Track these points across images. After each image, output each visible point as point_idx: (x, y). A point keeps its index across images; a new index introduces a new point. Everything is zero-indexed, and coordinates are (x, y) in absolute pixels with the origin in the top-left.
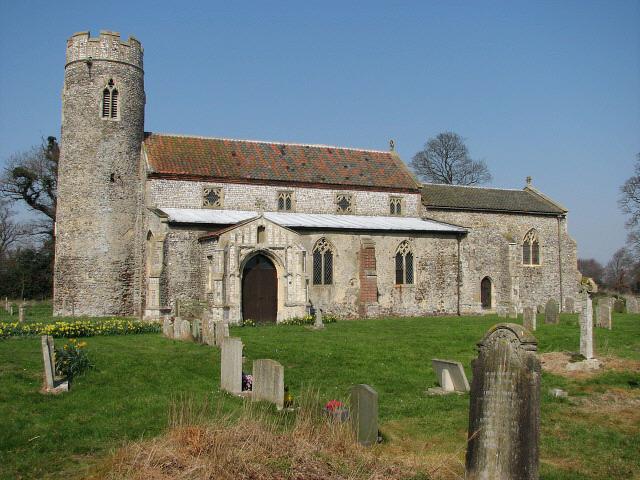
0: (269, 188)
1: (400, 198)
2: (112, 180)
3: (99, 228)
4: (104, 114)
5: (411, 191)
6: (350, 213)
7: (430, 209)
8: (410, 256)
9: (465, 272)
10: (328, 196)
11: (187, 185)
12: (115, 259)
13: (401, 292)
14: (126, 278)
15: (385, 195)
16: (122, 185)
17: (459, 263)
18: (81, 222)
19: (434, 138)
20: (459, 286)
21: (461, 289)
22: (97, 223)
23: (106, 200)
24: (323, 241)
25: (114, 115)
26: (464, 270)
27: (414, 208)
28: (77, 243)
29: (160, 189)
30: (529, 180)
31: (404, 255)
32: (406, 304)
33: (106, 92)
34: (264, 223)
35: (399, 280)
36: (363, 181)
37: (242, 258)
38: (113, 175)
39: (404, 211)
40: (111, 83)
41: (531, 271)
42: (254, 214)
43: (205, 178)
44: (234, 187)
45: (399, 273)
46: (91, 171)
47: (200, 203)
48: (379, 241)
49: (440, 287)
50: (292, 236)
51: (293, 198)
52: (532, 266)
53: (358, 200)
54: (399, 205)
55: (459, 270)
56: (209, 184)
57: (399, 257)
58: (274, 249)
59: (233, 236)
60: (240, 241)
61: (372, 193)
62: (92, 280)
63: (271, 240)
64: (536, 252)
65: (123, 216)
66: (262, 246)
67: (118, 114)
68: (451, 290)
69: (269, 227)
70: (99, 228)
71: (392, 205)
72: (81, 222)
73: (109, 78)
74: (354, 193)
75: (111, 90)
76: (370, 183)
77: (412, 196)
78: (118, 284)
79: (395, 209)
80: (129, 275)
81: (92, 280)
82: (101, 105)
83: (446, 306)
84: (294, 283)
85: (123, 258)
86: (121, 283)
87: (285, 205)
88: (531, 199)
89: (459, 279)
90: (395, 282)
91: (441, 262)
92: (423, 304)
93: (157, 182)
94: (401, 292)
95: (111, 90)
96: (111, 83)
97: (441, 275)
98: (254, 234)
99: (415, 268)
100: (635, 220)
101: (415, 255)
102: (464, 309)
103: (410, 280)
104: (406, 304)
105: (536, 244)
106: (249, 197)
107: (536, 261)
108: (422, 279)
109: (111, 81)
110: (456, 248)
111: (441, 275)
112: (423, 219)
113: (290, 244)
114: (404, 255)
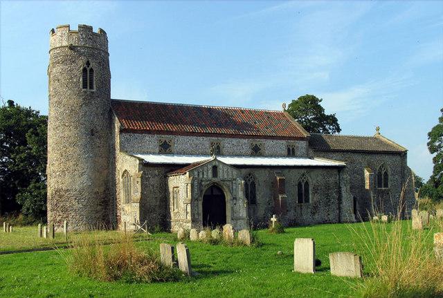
0: (205, 139)
8: (307, 184)
9: (344, 194)
11: (147, 137)
15: (284, 142)
19: (296, 99)
21: (341, 205)
24: (250, 175)
25: (91, 87)
27: (304, 151)
30: (378, 129)
33: (85, 70)
34: (217, 163)
35: (300, 201)
37: (205, 189)
38: (92, 130)
39: (298, 153)
41: (383, 192)
42: (211, 158)
44: (181, 138)
45: (300, 195)
48: (257, 173)
49: (327, 204)
50: (235, 172)
51: (221, 146)
53: (266, 146)
55: (339, 193)
57: (300, 185)
58: (224, 181)
60: (201, 176)
61: (275, 141)
65: (100, 160)
66: (215, 180)
68: (334, 207)
71: (289, 150)
74: (263, 141)
75: (88, 69)
76: (274, 134)
77: (302, 142)
78: (99, 208)
85: (102, 189)
88: (381, 142)
91: (328, 187)
92: (316, 216)
96: (88, 64)
98: (210, 172)
99: (310, 192)
101: (310, 184)
102: (214, 194)
103: (307, 201)
105: (386, 174)
107: (386, 185)
108: (315, 199)
109: (88, 62)
110: (338, 178)
113: (234, 177)
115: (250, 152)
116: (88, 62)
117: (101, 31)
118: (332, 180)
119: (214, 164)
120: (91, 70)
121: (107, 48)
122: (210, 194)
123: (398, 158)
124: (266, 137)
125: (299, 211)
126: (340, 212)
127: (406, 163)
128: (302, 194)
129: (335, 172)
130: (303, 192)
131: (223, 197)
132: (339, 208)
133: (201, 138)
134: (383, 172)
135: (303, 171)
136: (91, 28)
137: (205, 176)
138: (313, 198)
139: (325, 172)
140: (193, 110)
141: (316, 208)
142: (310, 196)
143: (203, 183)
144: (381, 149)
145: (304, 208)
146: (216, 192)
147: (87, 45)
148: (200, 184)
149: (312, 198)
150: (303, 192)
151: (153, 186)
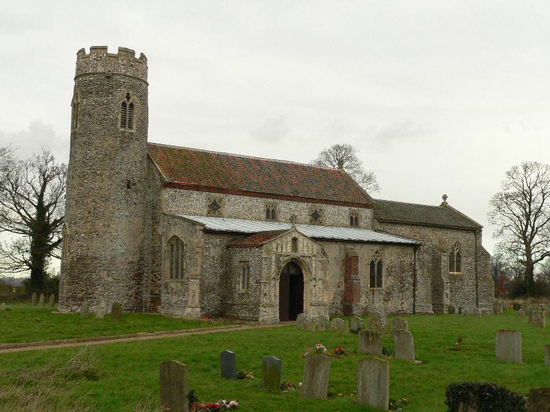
0: (260, 200)
1: (275, 205)
2: (128, 187)
3: (117, 231)
4: (123, 124)
5: (367, 206)
6: (321, 224)
7: (382, 222)
8: (380, 263)
10: (260, 204)
11: (195, 194)
12: (130, 259)
13: (373, 293)
14: (138, 277)
15: (346, 209)
16: (136, 191)
17: (415, 270)
18: (99, 225)
20: (414, 290)
21: (416, 292)
22: (114, 226)
23: (123, 206)
26: (418, 277)
28: (96, 244)
29: (173, 198)
30: (445, 197)
31: (376, 263)
32: (377, 305)
33: (124, 104)
34: (296, 235)
35: (372, 285)
36: (329, 194)
40: (128, 97)
41: (454, 277)
43: (209, 189)
44: (232, 198)
45: (372, 278)
46: (110, 178)
47: (205, 210)
48: (358, 250)
51: (277, 210)
52: (455, 273)
54: (273, 211)
55: (414, 276)
56: (213, 194)
57: (372, 264)
58: (303, 256)
59: (275, 246)
60: (279, 250)
62: (110, 279)
63: (305, 248)
64: (459, 261)
67: (134, 127)
68: (409, 293)
69: (300, 239)
70: (117, 231)
72: (99, 225)
73: (126, 92)
74: (324, 206)
75: (128, 104)
76: (335, 198)
78: (132, 282)
79: (354, 222)
80: (140, 274)
81: (110, 279)
82: (119, 117)
83: (406, 306)
84: (317, 287)
85: (136, 259)
86: (134, 282)
87: (316, 218)
89: (414, 285)
90: (369, 286)
92: (389, 305)
93: (171, 191)
94: (373, 293)
95: (128, 104)
97: (402, 281)
98: (290, 244)
100: (501, 232)
103: (380, 285)
104: (377, 305)
106: (243, 207)
107: (458, 270)
109: (128, 94)
110: (413, 257)
111: (402, 281)
112: (375, 231)
114: (376, 263)
115: (308, 219)
116: (128, 94)
117: (143, 56)
118: (408, 260)
119: (293, 236)
120: (132, 105)
121: (145, 74)
122: (286, 272)
123: (471, 236)
124: (327, 202)
125: (370, 297)
126: (414, 300)
127: (481, 242)
128: (454, 261)
129: (411, 251)
130: (376, 274)
131: (302, 275)
132: (414, 296)
133: (254, 199)
134: (456, 253)
135: (376, 248)
136: (133, 53)
137: (283, 250)
138: (386, 282)
139: (399, 250)
140: (483, 253)
141: (388, 294)
142: (383, 279)
143: (281, 259)
144: (452, 223)
145: (376, 294)
146: (293, 271)
147: (128, 74)
148: (278, 260)
149: (387, 281)
150: (376, 274)
151: (213, 258)
